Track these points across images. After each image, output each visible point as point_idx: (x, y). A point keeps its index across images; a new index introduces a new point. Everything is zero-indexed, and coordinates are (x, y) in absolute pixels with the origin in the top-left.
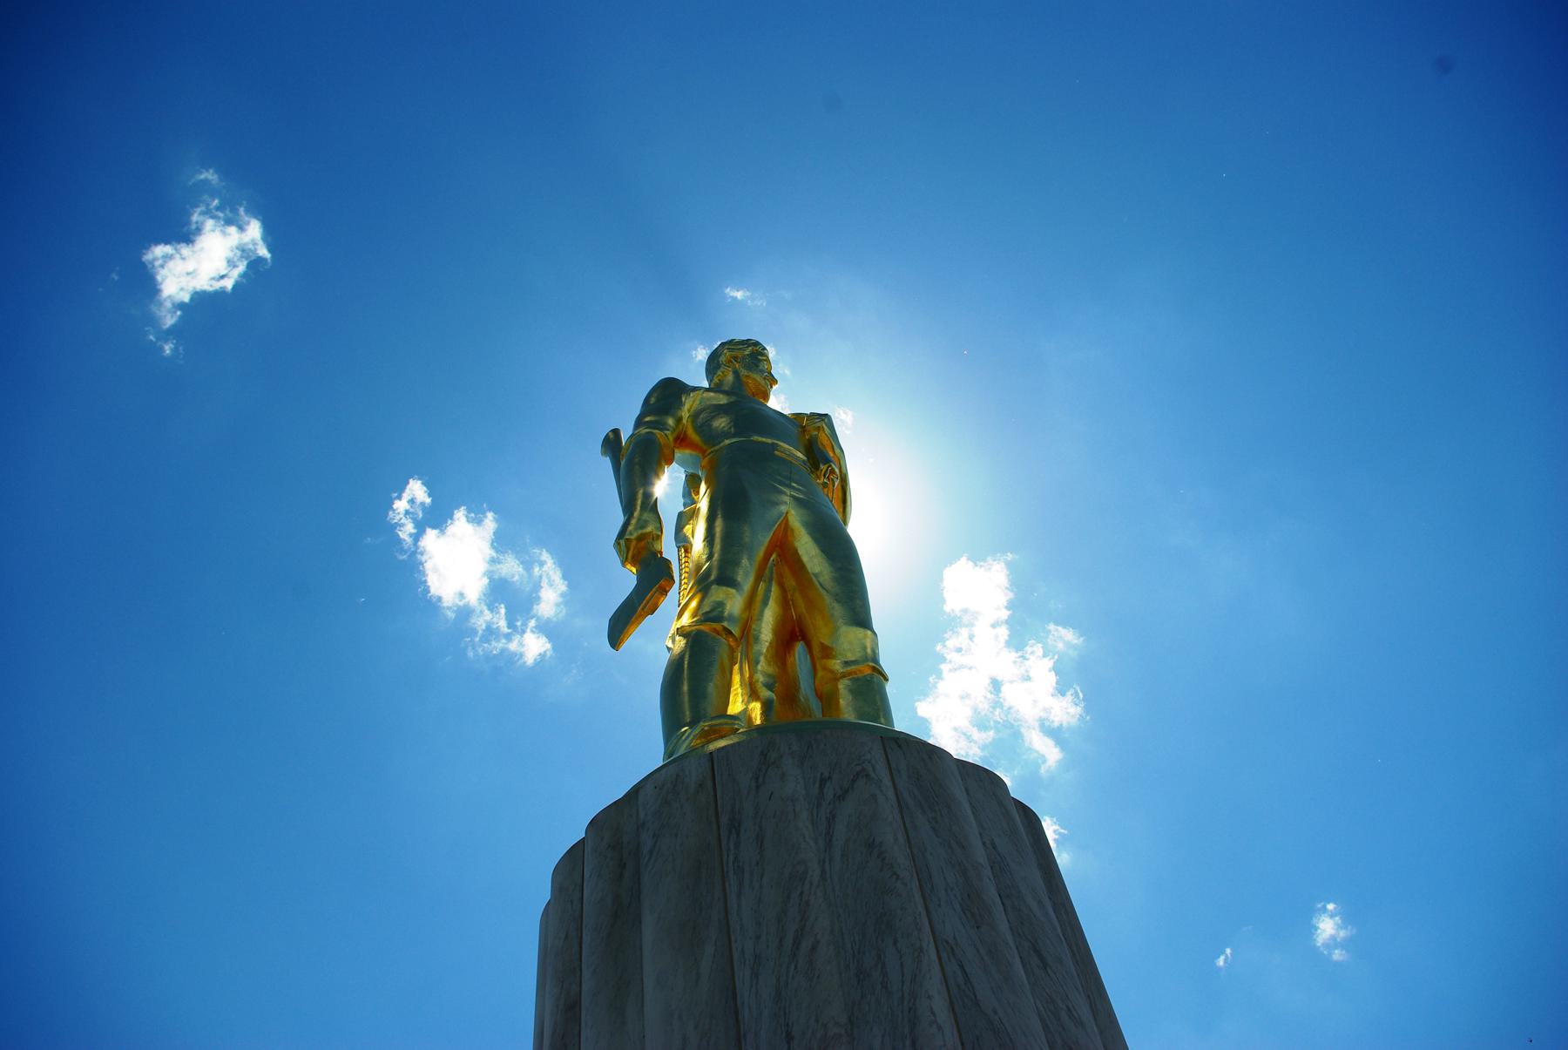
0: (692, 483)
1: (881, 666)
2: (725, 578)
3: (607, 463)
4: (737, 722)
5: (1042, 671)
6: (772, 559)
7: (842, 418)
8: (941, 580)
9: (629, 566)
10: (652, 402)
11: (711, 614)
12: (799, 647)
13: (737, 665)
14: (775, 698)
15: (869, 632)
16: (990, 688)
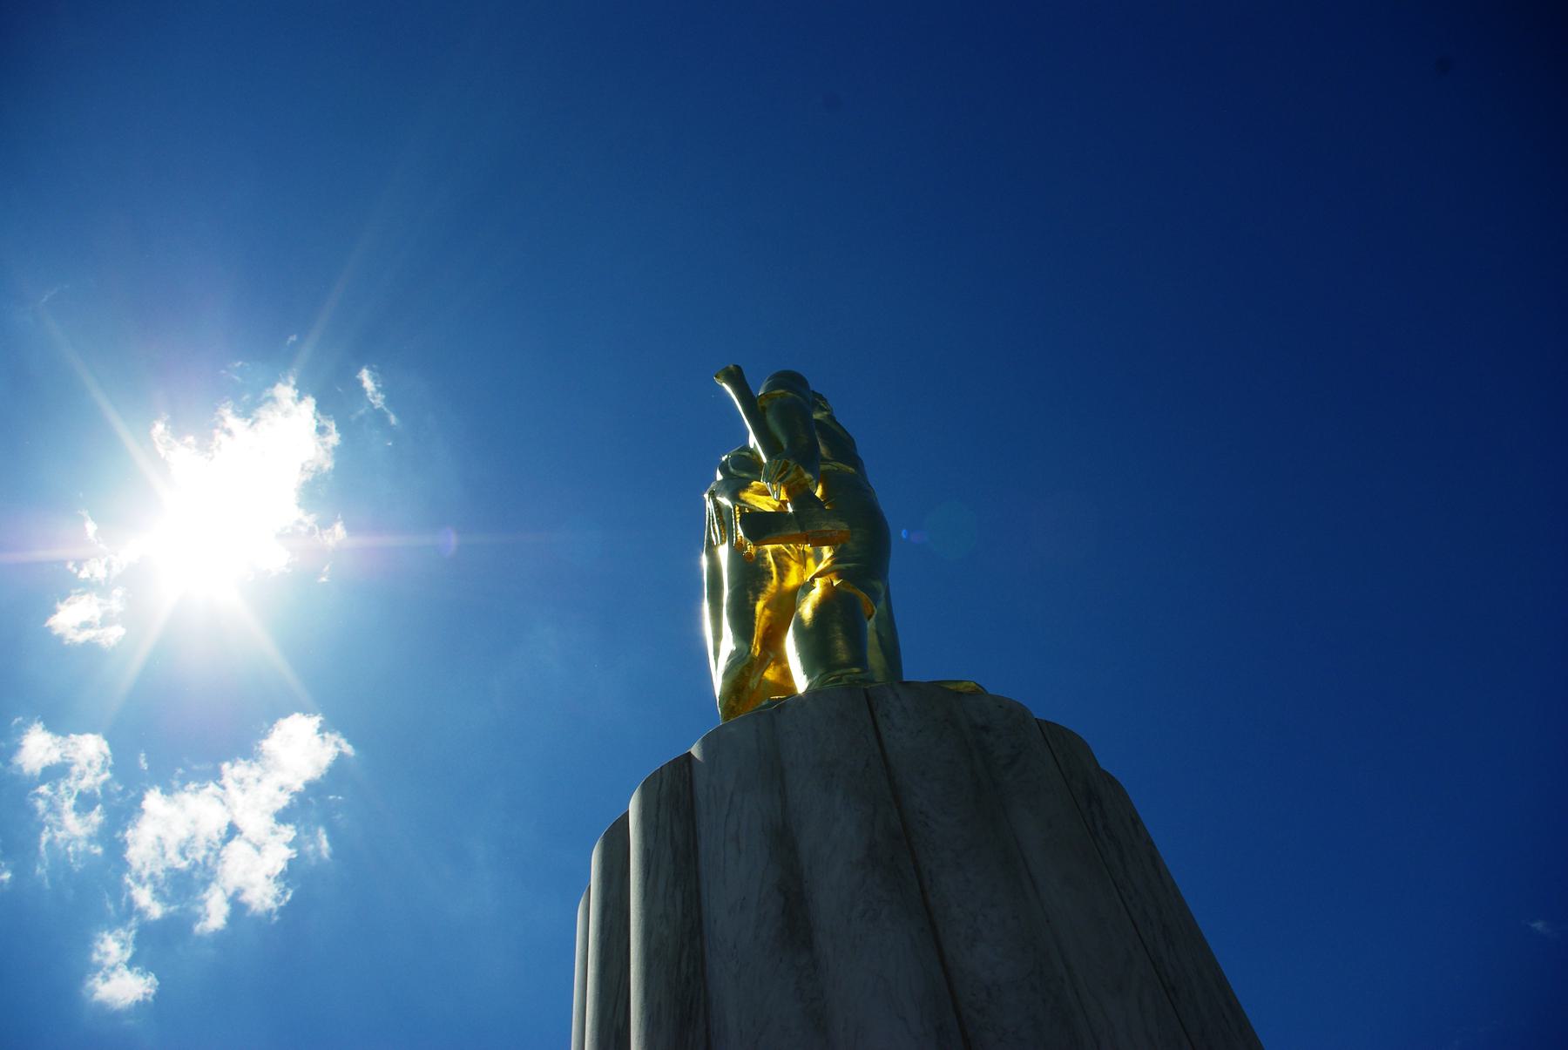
5: (278, 856)
7: (771, 498)
8: (286, 716)
10: (904, 531)
16: (223, 831)
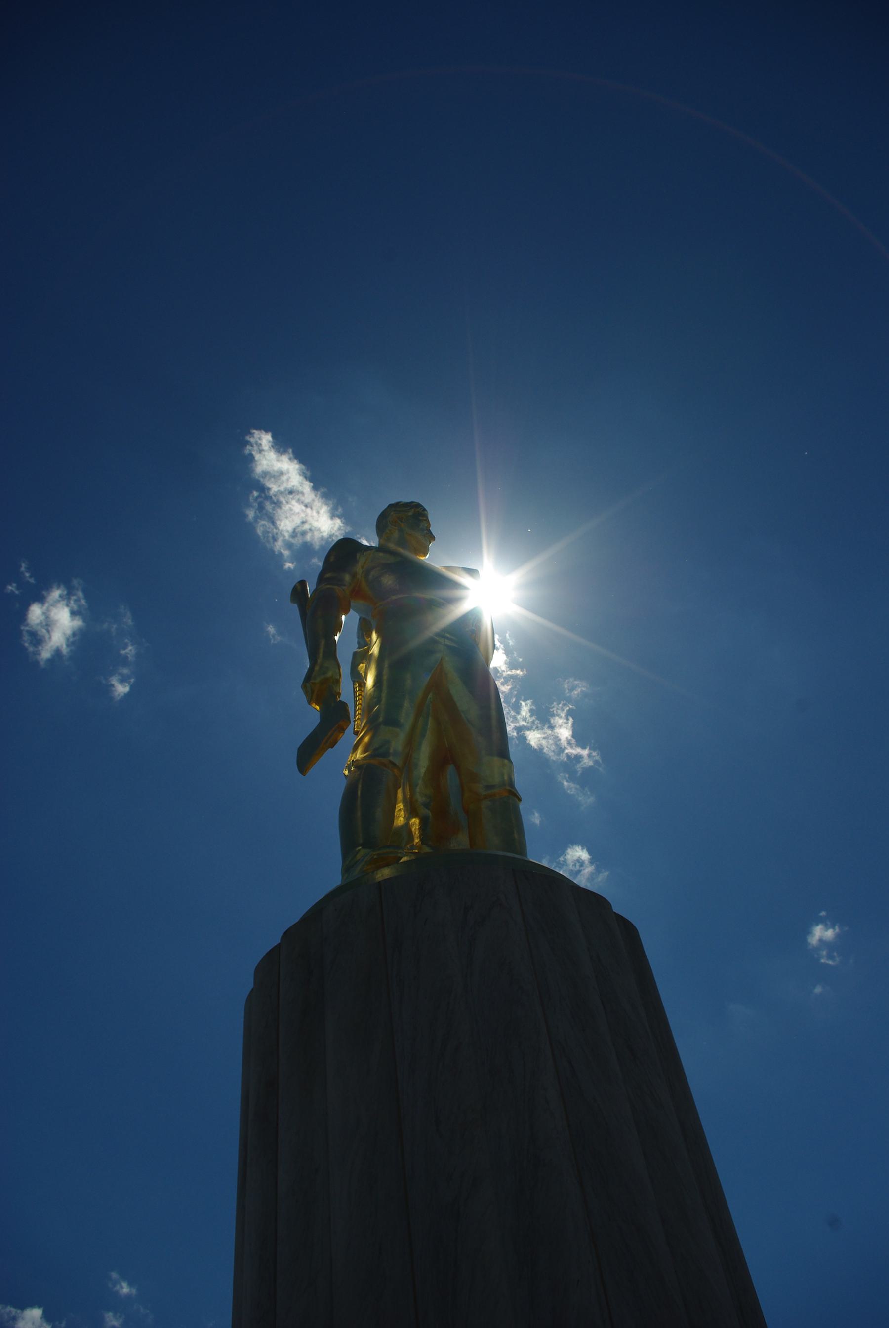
0: (364, 630)
1: (516, 790)
2: (392, 721)
3: (294, 609)
4: (399, 851)
6: (429, 697)
9: (314, 705)
11: (377, 751)
12: (451, 768)
13: (401, 789)
14: (430, 815)
15: (506, 761)
